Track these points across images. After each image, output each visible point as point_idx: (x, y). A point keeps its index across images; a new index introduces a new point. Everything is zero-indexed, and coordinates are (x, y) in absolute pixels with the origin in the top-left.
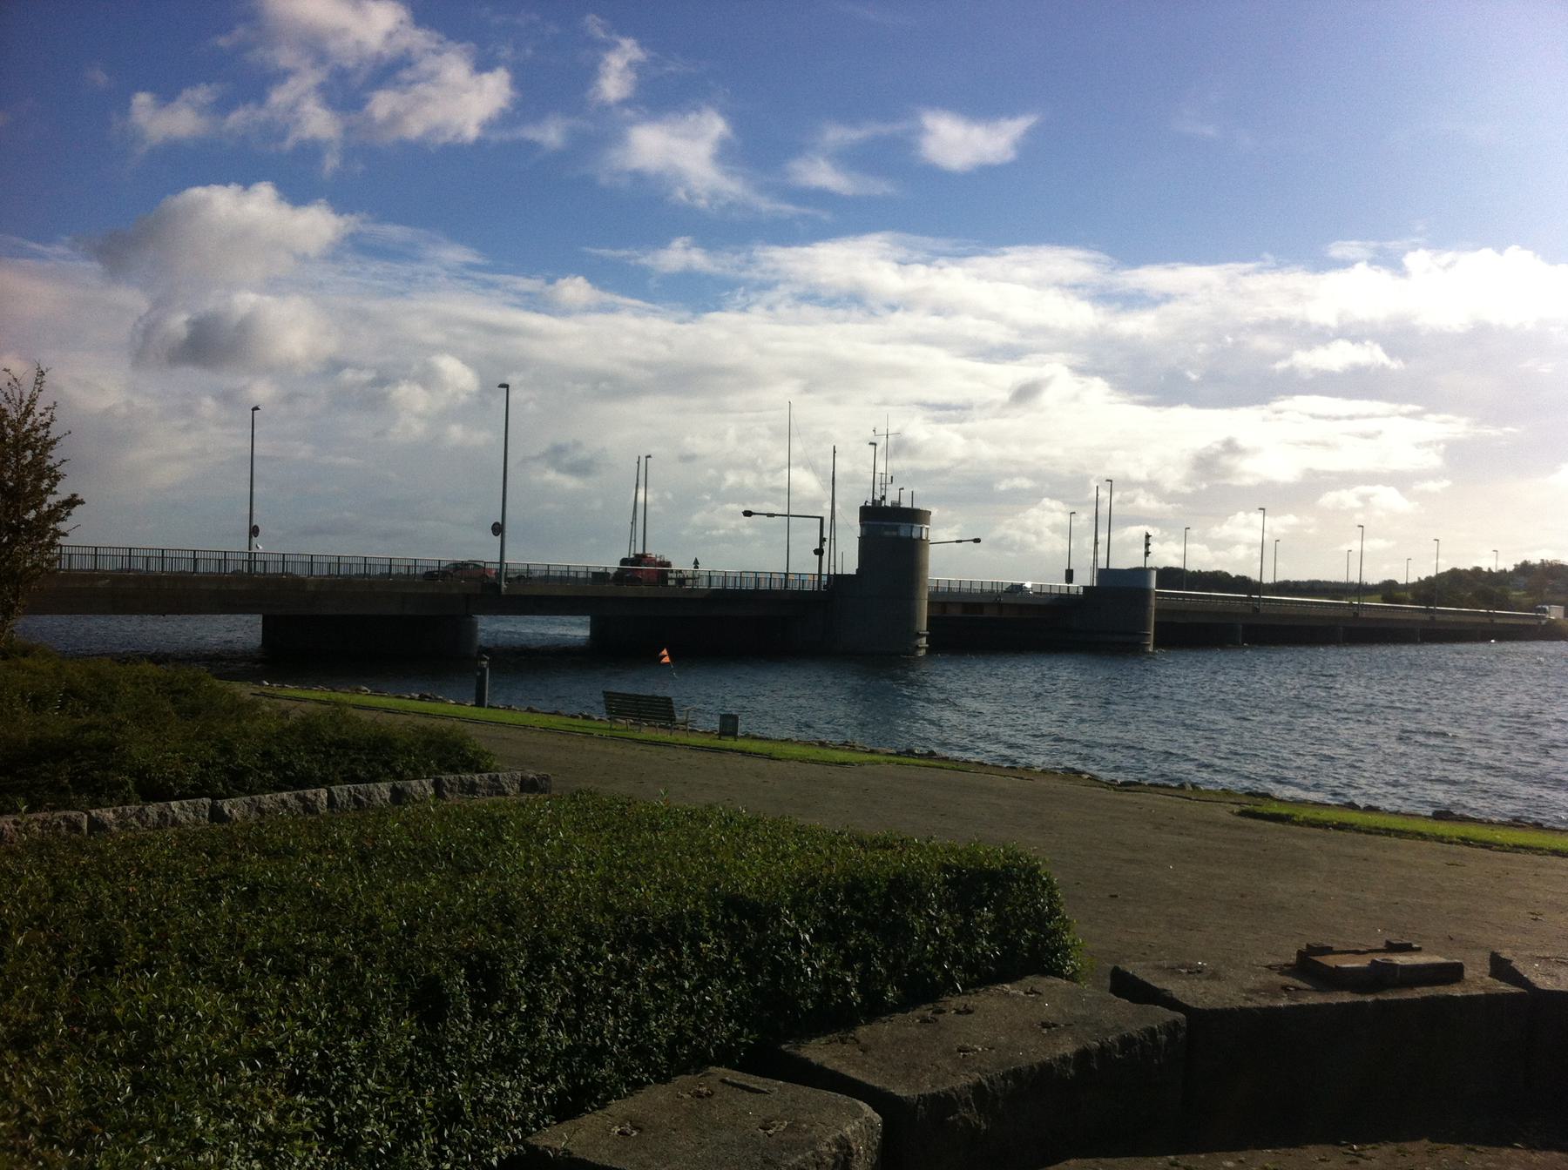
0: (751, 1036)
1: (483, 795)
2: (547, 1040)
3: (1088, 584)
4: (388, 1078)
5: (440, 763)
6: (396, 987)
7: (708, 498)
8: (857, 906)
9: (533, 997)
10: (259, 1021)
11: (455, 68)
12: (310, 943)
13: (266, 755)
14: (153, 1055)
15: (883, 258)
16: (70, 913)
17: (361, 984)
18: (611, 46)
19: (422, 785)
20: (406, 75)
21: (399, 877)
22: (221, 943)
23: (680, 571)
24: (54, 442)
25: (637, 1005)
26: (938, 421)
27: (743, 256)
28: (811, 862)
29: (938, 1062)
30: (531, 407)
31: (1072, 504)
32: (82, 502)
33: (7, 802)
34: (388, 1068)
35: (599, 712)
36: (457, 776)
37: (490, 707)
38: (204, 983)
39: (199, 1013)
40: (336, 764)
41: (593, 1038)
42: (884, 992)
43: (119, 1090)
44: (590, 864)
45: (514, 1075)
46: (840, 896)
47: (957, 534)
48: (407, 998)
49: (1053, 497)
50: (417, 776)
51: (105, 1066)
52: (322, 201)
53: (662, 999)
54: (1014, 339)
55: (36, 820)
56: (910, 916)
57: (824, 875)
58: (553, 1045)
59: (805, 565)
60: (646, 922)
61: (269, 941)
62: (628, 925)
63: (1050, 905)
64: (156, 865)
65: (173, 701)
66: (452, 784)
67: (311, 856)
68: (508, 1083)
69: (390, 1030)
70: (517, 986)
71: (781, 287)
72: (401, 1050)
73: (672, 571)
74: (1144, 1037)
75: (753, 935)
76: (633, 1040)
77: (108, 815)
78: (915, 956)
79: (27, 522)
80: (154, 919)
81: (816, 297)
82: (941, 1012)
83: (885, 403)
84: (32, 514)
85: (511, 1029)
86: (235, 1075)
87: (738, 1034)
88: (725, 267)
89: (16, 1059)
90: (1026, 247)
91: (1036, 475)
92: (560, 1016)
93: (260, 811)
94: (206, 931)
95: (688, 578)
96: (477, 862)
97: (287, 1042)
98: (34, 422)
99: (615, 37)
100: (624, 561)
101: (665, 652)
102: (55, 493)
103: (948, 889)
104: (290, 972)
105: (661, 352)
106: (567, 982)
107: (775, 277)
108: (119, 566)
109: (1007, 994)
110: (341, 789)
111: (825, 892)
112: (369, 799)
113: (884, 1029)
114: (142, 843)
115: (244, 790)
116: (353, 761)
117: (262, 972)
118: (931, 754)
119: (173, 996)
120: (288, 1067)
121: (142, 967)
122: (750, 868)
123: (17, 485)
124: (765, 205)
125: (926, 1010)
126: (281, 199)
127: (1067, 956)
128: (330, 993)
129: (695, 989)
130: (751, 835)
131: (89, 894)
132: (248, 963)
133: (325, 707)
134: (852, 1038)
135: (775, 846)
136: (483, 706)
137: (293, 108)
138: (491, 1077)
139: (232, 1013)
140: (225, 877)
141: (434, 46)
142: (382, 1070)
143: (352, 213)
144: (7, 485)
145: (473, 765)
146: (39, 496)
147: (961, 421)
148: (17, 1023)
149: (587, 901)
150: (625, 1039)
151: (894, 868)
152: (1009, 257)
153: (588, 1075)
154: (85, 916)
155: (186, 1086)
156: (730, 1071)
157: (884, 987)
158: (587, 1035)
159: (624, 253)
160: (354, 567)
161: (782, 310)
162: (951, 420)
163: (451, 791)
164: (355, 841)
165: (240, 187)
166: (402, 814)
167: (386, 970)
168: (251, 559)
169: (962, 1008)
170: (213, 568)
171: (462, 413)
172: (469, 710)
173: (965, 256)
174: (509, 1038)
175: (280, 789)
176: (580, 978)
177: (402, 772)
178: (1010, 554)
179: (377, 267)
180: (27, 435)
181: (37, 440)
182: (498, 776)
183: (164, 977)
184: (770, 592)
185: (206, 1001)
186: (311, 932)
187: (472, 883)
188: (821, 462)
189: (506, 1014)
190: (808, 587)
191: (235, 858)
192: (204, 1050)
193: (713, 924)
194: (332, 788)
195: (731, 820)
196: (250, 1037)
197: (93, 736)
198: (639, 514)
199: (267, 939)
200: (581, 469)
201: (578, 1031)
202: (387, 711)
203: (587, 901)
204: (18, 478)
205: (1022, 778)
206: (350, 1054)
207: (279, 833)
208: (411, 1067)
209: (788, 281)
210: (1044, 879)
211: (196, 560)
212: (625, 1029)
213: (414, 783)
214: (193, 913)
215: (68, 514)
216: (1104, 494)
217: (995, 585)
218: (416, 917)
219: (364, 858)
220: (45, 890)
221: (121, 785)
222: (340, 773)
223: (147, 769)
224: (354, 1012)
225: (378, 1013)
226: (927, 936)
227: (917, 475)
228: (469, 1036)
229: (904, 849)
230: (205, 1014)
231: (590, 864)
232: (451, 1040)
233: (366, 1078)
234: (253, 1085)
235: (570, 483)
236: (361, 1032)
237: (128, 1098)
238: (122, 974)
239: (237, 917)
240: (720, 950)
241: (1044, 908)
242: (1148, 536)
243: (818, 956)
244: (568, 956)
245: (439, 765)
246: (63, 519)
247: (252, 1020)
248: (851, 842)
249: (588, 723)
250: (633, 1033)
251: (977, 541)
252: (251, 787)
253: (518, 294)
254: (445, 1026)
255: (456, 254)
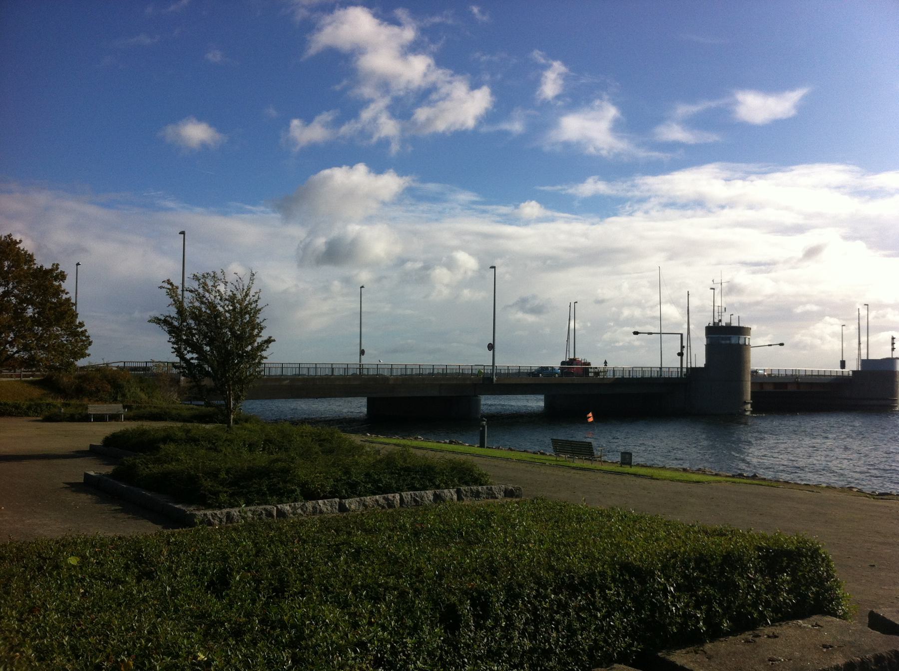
0: (639, 647)
1: (484, 498)
2: (517, 643)
3: (855, 369)
4: (429, 661)
5: (460, 479)
6: (432, 609)
7: (612, 324)
8: (703, 571)
9: (509, 618)
10: (359, 626)
11: (460, 89)
12: (387, 583)
13: (368, 475)
14: (303, 643)
15: (716, 178)
16: (264, 563)
17: (413, 606)
18: (546, 67)
19: (450, 492)
20: (434, 96)
21: (435, 545)
22: (340, 581)
23: (596, 368)
24: (260, 310)
25: (569, 627)
26: (754, 273)
27: (629, 183)
28: (674, 543)
29: (755, 667)
30: (507, 276)
31: (844, 320)
32: (274, 341)
33: (236, 500)
34: (428, 655)
35: (550, 451)
36: (469, 487)
37: (487, 447)
38: (331, 603)
39: (327, 621)
40: (404, 480)
41: (544, 644)
42: (721, 623)
43: (285, 662)
44: (541, 541)
45: (499, 663)
46: (692, 565)
47: (770, 341)
48: (438, 615)
49: (831, 316)
50: (447, 487)
51: (279, 649)
52: (391, 170)
53: (584, 623)
54: (800, 221)
55: (250, 510)
56: (737, 578)
57: (682, 551)
58: (521, 646)
59: (672, 363)
60: (573, 577)
61: (365, 580)
62: (563, 578)
63: (827, 571)
64: (308, 536)
65: (320, 445)
66: (467, 492)
67: (388, 532)
68: (496, 668)
69: (429, 634)
70: (499, 611)
71: (652, 199)
72: (435, 645)
73: (591, 368)
74: (890, 656)
75: (638, 587)
76: (568, 646)
77: (287, 508)
78: (740, 602)
79: (247, 352)
80: (306, 567)
81: (676, 204)
82: (758, 636)
83: (719, 264)
84: (250, 348)
85: (497, 636)
86: (346, 656)
87: (632, 645)
88: (618, 190)
89: (234, 642)
90: (805, 165)
91: (819, 303)
92: (525, 630)
93: (364, 505)
94: (332, 574)
95: (601, 372)
96: (477, 539)
97: (373, 638)
98: (250, 300)
99: (550, 62)
100: (563, 363)
101: (590, 415)
102: (261, 336)
103: (761, 562)
104: (376, 599)
105: (583, 241)
106: (529, 611)
107: (649, 194)
108: (294, 373)
109: (800, 626)
110: (407, 494)
111: (682, 562)
112: (421, 499)
113: (723, 646)
114: (302, 524)
115: (356, 494)
116: (413, 478)
117: (360, 598)
118: (754, 477)
119: (314, 610)
120: (374, 653)
121: (299, 593)
122: (636, 546)
123: (241, 333)
124: (642, 154)
125: (748, 635)
126: (370, 172)
127: (839, 604)
128: (397, 611)
129: (604, 617)
130: (637, 526)
131: (273, 552)
132: (354, 592)
133: (397, 448)
134: (701, 650)
135: (652, 533)
136: (484, 447)
137: (375, 119)
138: (486, 663)
139: (344, 621)
140: (343, 544)
141: (448, 79)
142: (425, 656)
143: (407, 175)
144: (236, 333)
145: (477, 481)
146: (252, 338)
147: (769, 272)
148: (235, 623)
149: (539, 563)
150: (563, 645)
151: (726, 548)
152: (794, 172)
153: (542, 665)
154: (272, 565)
155: (320, 661)
156: (627, 667)
157: (721, 620)
158: (540, 642)
159: (559, 187)
160: (414, 370)
161: (653, 213)
162: (762, 272)
163: (466, 496)
164: (412, 525)
165: (348, 167)
166: (437, 510)
167: (427, 599)
168: (361, 367)
169: (771, 634)
170: (342, 372)
171: (471, 283)
172: (476, 449)
173: (766, 173)
174: (496, 641)
175: (375, 494)
176: (535, 609)
177: (439, 485)
178: (805, 352)
179: (424, 206)
180: (246, 307)
181: (251, 309)
182: (491, 488)
183: (310, 599)
184: (651, 378)
185: (331, 613)
186: (388, 576)
187: (474, 550)
188: (682, 300)
189: (494, 627)
190: (674, 375)
191: (349, 533)
192: (329, 641)
193: (614, 580)
194: (402, 493)
195: (626, 517)
196: (354, 635)
197: (279, 465)
198: (571, 336)
199: (364, 579)
200: (537, 310)
201: (535, 639)
202: (432, 450)
203: (539, 563)
204: (242, 329)
205: (813, 491)
206: (408, 647)
207: (372, 519)
208: (441, 655)
209: (656, 196)
210: (823, 555)
211: (333, 369)
212: (563, 639)
213: (446, 491)
214: (326, 563)
215: (267, 347)
216: (863, 312)
217: (797, 372)
218: (444, 569)
219: (416, 534)
220: (251, 550)
221: (293, 491)
222: (406, 485)
223: (306, 483)
224: (409, 623)
225: (422, 624)
226: (748, 590)
227: (743, 306)
228: (473, 639)
229: (733, 537)
230: (330, 621)
231: (541, 541)
232: (463, 641)
233: (416, 660)
234: (356, 662)
235: (531, 318)
236: (413, 634)
237: (290, 667)
238: (288, 597)
239: (349, 567)
240: (618, 595)
241: (823, 573)
242: (893, 338)
243: (679, 600)
244: (528, 595)
245: (459, 481)
246: (265, 350)
247: (355, 626)
248: (699, 531)
249: (543, 457)
250: (568, 642)
251: (782, 344)
252: (360, 493)
253: (499, 215)
254: (460, 632)
255: (465, 197)
